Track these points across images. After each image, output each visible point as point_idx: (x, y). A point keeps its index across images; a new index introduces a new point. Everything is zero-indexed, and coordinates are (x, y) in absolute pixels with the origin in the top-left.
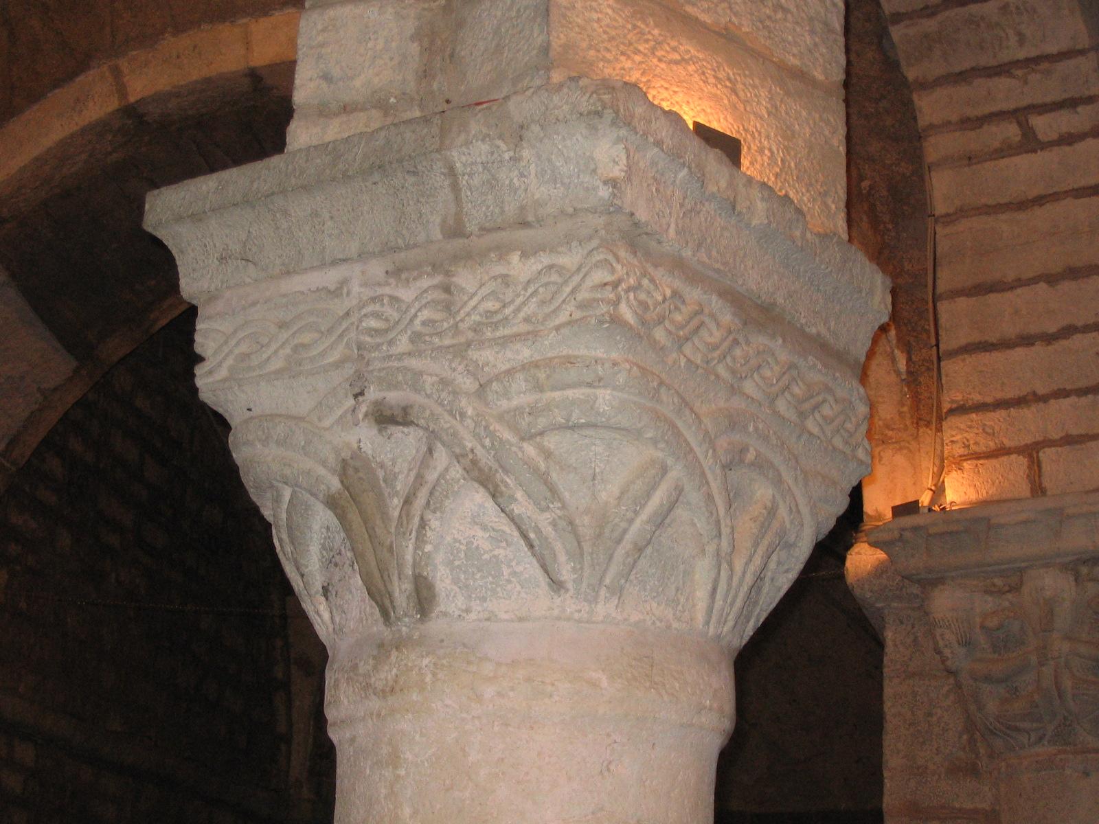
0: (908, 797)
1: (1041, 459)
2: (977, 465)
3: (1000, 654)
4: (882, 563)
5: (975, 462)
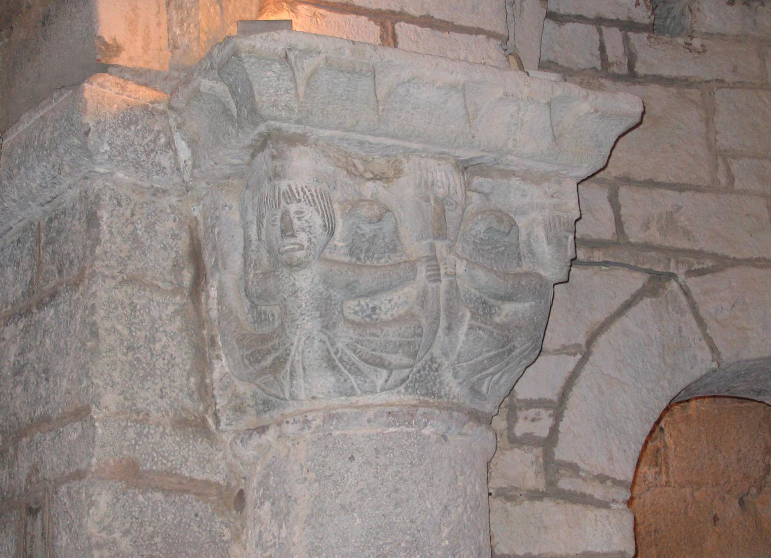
0: (125, 452)
1: (397, 32)
2: (314, 14)
3: (359, 259)
4: (607, 26)
5: (314, 9)
